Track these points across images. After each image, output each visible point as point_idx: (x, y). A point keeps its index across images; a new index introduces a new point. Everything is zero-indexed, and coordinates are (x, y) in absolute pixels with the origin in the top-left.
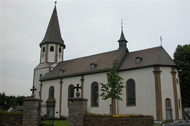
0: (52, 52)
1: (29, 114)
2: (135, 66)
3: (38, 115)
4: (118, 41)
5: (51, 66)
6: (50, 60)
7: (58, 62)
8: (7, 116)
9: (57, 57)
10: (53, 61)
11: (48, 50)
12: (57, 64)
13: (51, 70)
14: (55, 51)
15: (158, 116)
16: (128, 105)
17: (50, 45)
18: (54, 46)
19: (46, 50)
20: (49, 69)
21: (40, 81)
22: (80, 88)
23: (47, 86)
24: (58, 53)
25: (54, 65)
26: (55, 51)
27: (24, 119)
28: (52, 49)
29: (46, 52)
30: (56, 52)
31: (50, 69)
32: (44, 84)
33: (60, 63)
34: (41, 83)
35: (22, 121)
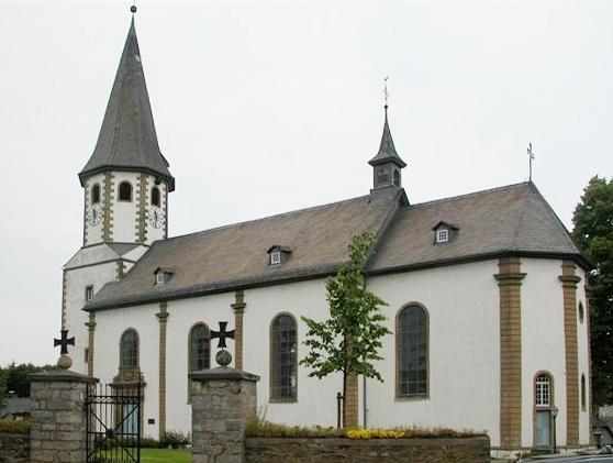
0: (125, 204)
1: (52, 427)
4: (370, 163)
5: (124, 257)
7: (149, 242)
9: (147, 221)
10: (133, 239)
13: (125, 271)
14: (137, 199)
17: (118, 178)
18: (133, 179)
19: (102, 198)
21: (85, 309)
23: (112, 327)
24: (150, 207)
25: (136, 254)
26: (137, 199)
29: (103, 206)
30: (142, 204)
31: (122, 267)
32: (102, 320)
33: (155, 243)
34: (92, 317)
35: (28, 449)
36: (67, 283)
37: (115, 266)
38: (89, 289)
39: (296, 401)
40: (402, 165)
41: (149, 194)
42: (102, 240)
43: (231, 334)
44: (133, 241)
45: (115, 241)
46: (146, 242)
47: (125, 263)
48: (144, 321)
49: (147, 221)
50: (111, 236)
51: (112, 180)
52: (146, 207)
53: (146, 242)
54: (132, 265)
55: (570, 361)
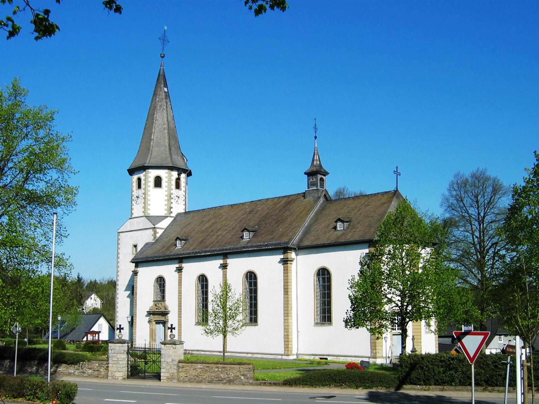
0: (158, 190)
1: (116, 359)
2: (332, 237)
3: (127, 359)
4: (305, 173)
5: (156, 226)
6: (153, 212)
7: (174, 214)
8: (219, 365)
9: (172, 201)
10: (163, 213)
11: (150, 186)
12: (173, 219)
13: (158, 235)
14: (166, 186)
15: (373, 348)
16: (324, 324)
17: (153, 173)
18: (163, 173)
19: (143, 186)
20: (153, 233)
21: (132, 262)
22: (169, 328)
23: (148, 275)
24: (175, 191)
25: (165, 224)
26: (166, 186)
27: (110, 365)
28: (158, 182)
29: (143, 191)
30: (170, 189)
31: (155, 233)
32: (143, 271)
33: (179, 215)
34: (136, 266)
35: (108, 367)
36: (119, 251)
37: (151, 232)
38: (135, 246)
39: (317, 324)
40: (325, 174)
41: (174, 183)
42: (143, 215)
43: (169, 328)
44: (164, 215)
45: (151, 215)
46: (172, 215)
47: (158, 230)
48: (168, 271)
49: (172, 201)
50: (149, 212)
51: (149, 175)
52: (172, 192)
53: (172, 215)
54: (163, 230)
55: (286, 334)
